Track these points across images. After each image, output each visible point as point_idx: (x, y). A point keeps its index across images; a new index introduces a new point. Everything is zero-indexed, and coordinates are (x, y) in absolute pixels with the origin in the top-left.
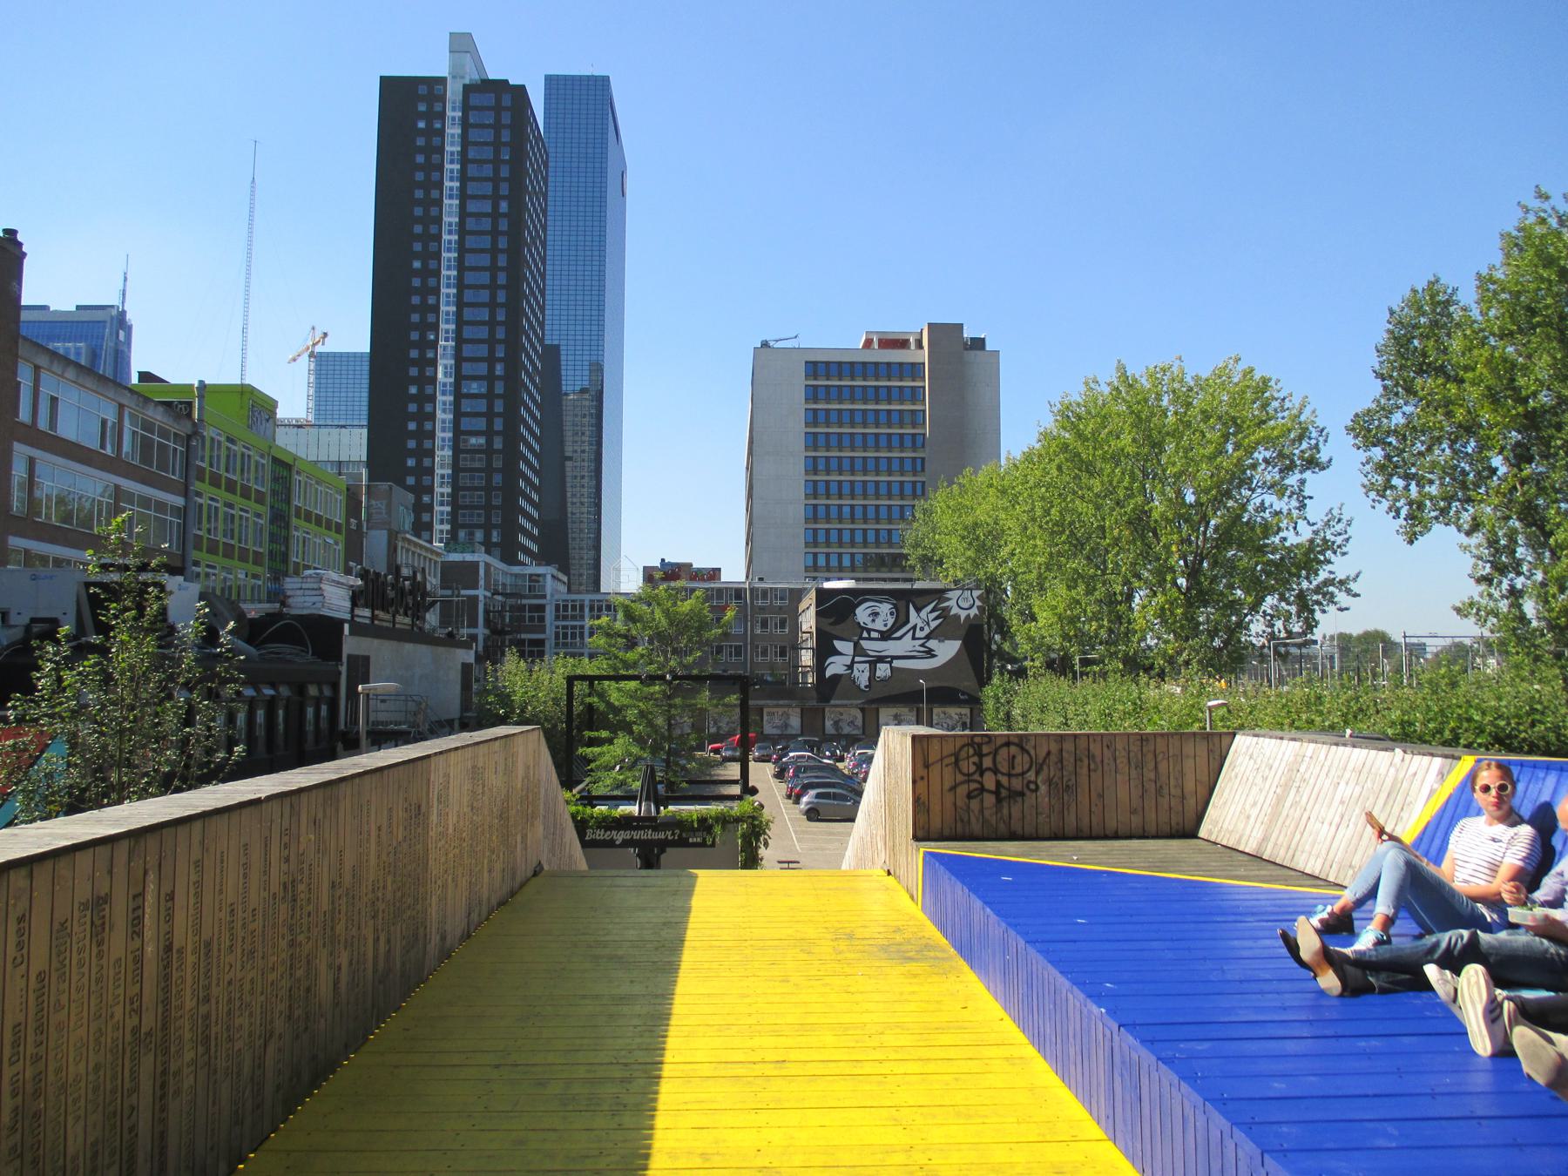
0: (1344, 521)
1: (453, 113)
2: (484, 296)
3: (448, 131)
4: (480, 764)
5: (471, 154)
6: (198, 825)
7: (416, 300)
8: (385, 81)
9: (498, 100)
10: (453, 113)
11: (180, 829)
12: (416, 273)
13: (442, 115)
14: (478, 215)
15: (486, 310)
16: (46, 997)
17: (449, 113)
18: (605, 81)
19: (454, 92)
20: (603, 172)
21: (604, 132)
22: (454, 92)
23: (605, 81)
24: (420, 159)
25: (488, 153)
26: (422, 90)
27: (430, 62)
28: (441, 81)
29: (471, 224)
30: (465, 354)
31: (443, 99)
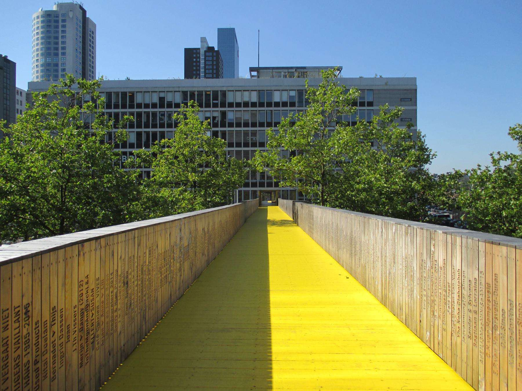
0: (93, 250)
1: (202, 57)
2: (211, 67)
3: (201, 62)
4: (193, 189)
5: (207, 67)
6: (62, 251)
7: (195, 72)
8: (186, 49)
9: (213, 54)
10: (202, 57)
11: (74, 246)
12: (194, 70)
13: (199, 58)
14: (209, 69)
15: (211, 57)
16: (34, 327)
17: (201, 57)
18: (234, 29)
19: (202, 52)
20: (234, 50)
21: (234, 43)
22: (202, 52)
23: (234, 29)
24: (195, 60)
25: (211, 67)
26: (195, 51)
27: (196, 44)
28: (199, 49)
29: (207, 71)
30: (207, 59)
31: (199, 53)
